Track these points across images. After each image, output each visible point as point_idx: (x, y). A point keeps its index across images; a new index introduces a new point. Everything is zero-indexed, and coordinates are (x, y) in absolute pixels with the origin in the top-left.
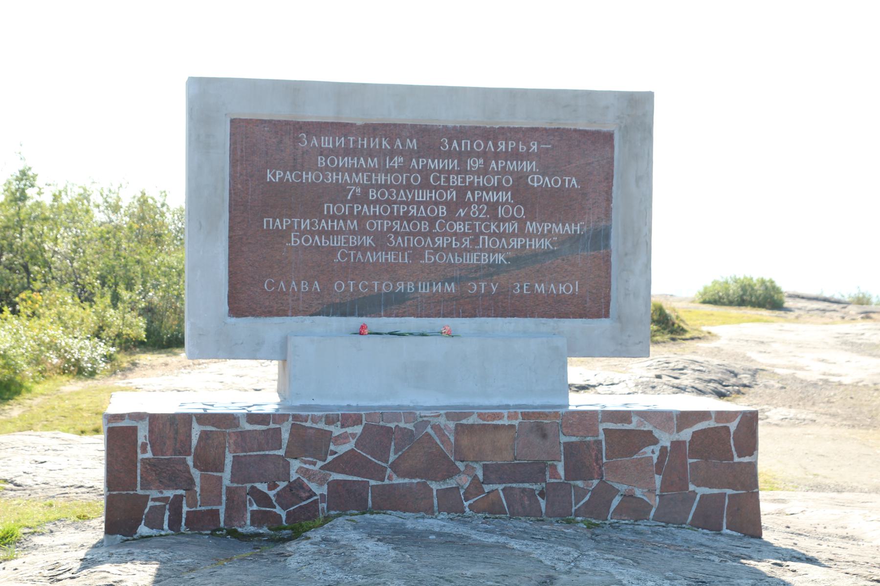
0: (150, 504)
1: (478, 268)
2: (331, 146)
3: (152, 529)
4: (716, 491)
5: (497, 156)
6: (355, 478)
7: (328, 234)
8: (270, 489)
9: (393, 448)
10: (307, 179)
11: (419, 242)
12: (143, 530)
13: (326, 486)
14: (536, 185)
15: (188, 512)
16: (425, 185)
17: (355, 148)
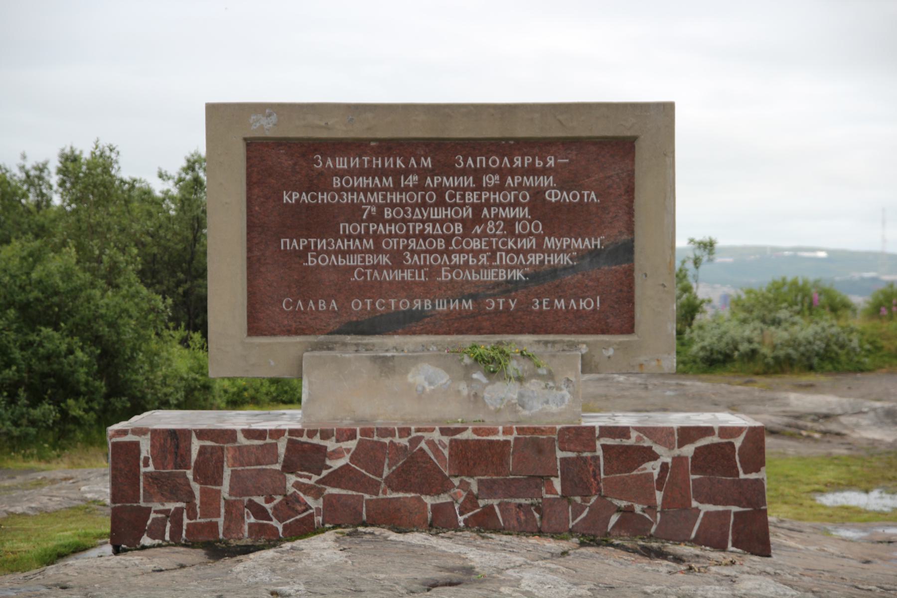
0: (153, 516)
1: (498, 284)
2: (346, 166)
3: (154, 539)
4: (720, 508)
5: (513, 172)
6: (350, 492)
7: (344, 253)
8: (267, 502)
9: (387, 461)
10: (323, 200)
11: (436, 260)
12: (146, 540)
13: (321, 500)
14: (553, 200)
15: (188, 525)
16: (441, 203)
17: (370, 168)
